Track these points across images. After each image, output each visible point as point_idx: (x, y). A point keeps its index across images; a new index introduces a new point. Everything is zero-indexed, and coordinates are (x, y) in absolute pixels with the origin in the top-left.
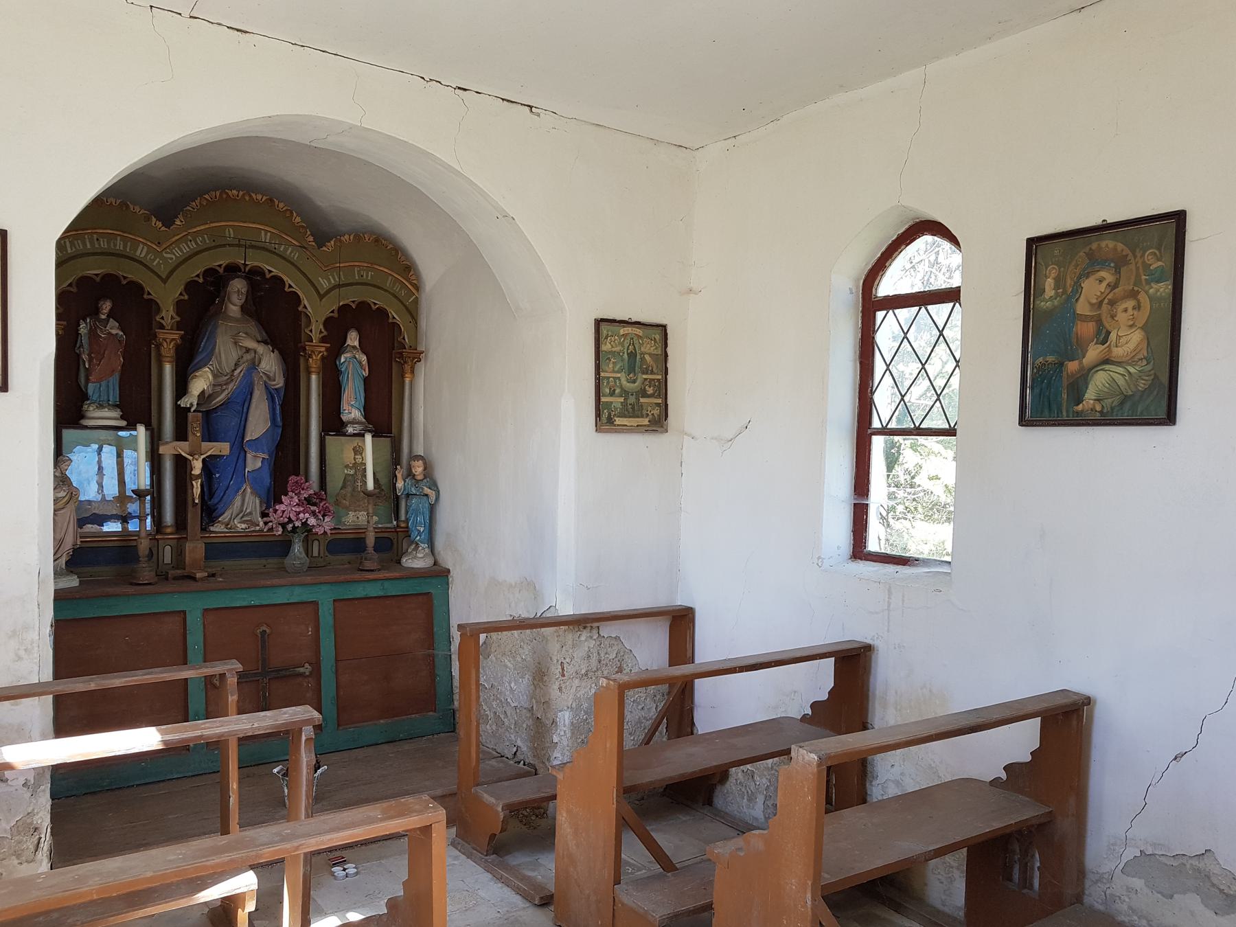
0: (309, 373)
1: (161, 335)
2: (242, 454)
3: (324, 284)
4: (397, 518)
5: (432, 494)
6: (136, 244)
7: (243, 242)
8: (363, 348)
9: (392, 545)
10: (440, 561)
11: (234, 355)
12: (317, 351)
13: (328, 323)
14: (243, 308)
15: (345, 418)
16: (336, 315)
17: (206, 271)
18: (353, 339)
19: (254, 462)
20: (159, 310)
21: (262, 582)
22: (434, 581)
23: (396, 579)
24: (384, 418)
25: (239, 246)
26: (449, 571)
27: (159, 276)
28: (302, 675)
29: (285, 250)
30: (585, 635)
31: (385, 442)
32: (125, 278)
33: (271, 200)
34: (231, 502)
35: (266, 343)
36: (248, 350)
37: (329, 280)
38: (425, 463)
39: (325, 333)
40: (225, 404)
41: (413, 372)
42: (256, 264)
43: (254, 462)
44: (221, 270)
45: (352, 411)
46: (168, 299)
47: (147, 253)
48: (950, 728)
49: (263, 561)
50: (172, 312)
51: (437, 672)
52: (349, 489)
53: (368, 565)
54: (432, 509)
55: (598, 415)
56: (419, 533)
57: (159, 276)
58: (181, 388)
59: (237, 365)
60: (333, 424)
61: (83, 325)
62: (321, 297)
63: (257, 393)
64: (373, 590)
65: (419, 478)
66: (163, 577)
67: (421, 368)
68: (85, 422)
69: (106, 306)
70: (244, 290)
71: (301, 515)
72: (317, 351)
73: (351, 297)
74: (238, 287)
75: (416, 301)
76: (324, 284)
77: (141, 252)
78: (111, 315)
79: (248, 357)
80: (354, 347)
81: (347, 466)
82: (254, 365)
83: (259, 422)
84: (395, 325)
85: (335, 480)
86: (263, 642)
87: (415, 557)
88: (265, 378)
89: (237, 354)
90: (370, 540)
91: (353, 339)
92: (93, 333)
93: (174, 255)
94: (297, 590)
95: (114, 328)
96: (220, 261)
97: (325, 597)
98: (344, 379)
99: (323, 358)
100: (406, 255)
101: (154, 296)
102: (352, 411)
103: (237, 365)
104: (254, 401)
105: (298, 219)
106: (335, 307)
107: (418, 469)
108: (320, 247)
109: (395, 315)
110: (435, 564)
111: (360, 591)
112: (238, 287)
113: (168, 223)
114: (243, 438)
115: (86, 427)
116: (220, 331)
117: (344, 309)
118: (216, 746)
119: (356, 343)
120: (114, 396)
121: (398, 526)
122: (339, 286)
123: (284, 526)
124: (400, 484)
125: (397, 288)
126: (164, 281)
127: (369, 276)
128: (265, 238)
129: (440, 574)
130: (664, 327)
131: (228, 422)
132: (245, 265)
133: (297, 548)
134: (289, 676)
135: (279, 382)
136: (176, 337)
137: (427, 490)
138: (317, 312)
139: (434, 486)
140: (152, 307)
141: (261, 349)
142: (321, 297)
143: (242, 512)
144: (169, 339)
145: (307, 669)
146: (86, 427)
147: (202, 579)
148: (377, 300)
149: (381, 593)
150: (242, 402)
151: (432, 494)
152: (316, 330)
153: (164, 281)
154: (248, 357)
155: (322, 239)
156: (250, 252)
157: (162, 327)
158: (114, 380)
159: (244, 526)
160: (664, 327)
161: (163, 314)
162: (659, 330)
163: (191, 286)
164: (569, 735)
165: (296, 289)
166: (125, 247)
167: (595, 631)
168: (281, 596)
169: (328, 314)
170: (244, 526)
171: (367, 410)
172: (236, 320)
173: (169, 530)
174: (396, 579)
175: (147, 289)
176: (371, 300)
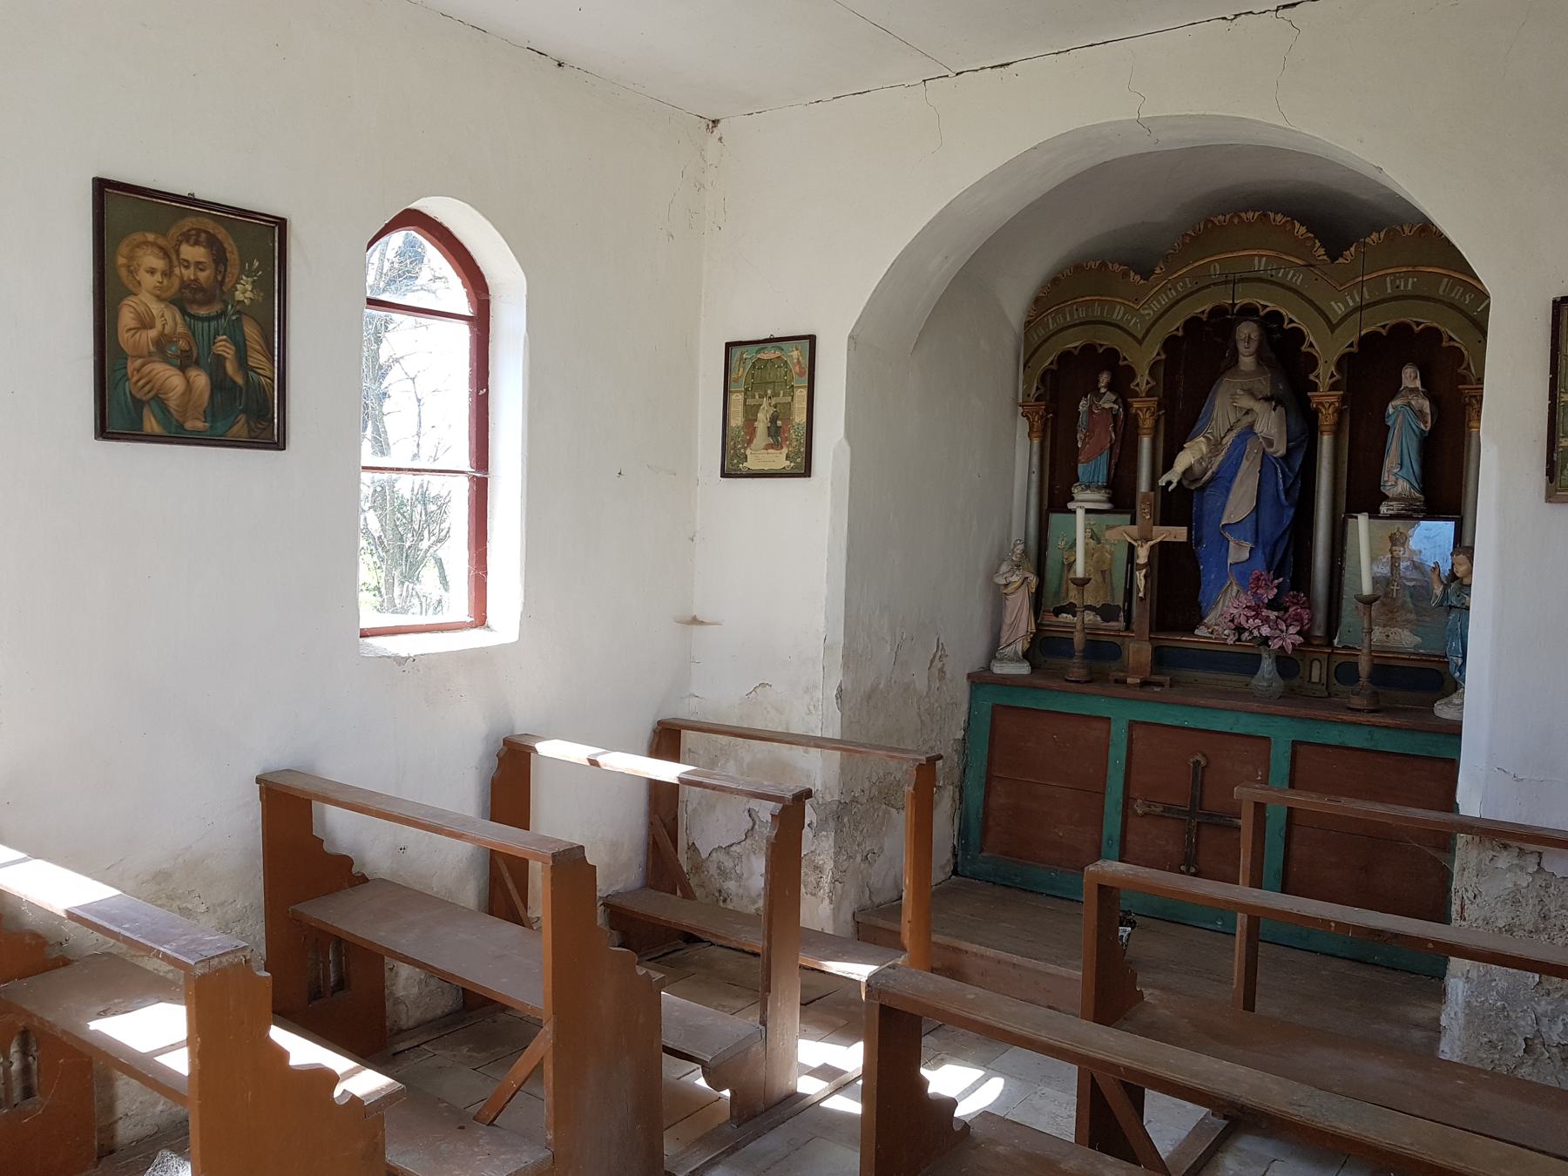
7: (1231, 277)
14: (1259, 355)
16: (1355, 349)
17: (1186, 323)
20: (1134, 376)
25: (1226, 282)
27: (1135, 337)
30: (1504, 860)
37: (1346, 304)
39: (1337, 377)
42: (1246, 301)
43: (1239, 552)
44: (1204, 317)
45: (1398, 480)
46: (1143, 358)
47: (1463, 294)
48: (1194, 1082)
50: (1146, 377)
55: (1551, 473)
57: (1135, 337)
59: (1230, 430)
63: (1245, 464)
64: (1355, 738)
69: (1104, 379)
72: (1326, 400)
73: (1379, 321)
74: (1247, 332)
76: (1339, 309)
77: (1118, 315)
78: (1110, 387)
80: (1413, 390)
83: (1240, 503)
86: (1195, 774)
89: (1242, 417)
90: (1364, 667)
93: (1149, 313)
94: (1244, 718)
95: (1108, 401)
97: (1281, 734)
102: (1398, 480)
103: (1230, 430)
106: (1355, 339)
111: (1333, 735)
112: (1247, 332)
113: (1146, 274)
116: (1221, 390)
118: (1227, 909)
119: (1418, 383)
120: (1102, 478)
125: (1456, 295)
126: (1140, 342)
128: (1259, 265)
130: (729, 346)
132: (1234, 305)
133: (1267, 665)
136: (1333, 399)
138: (1327, 351)
141: (1257, 407)
143: (1227, 611)
144: (1146, 411)
147: (1134, 685)
148: (1422, 318)
150: (1223, 480)
153: (1140, 342)
156: (1239, 287)
157: (1136, 394)
158: (1103, 460)
160: (729, 346)
162: (736, 352)
163: (1170, 344)
164: (1462, 1021)
167: (1534, 859)
169: (1343, 350)
172: (1247, 374)
174: (1398, 728)
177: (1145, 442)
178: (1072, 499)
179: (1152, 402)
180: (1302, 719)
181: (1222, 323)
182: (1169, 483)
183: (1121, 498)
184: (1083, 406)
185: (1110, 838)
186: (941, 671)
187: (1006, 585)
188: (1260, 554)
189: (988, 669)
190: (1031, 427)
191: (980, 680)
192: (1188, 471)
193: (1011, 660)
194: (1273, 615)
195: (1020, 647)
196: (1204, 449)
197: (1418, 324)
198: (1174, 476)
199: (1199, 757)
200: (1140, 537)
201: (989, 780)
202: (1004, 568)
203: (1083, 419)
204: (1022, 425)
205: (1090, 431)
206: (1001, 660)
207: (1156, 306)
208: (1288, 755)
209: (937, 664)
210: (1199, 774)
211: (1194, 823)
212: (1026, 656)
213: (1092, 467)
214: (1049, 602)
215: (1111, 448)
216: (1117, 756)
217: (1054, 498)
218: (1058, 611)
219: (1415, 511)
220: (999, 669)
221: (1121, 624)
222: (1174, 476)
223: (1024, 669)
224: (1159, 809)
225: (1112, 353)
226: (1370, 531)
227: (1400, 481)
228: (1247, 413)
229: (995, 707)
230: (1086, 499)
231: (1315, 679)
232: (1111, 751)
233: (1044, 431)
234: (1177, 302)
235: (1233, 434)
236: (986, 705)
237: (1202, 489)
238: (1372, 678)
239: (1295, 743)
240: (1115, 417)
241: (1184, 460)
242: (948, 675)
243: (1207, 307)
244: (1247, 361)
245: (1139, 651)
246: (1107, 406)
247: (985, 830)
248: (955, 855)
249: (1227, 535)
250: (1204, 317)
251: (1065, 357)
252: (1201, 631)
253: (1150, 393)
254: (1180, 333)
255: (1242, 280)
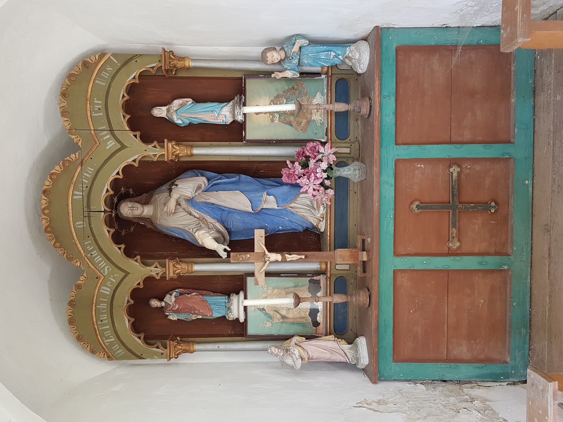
0: (192, 155)
1: (171, 274)
2: (263, 211)
3: (111, 144)
4: (319, 74)
5: (300, 42)
6: (100, 295)
7: (86, 214)
8: (166, 103)
9: (344, 83)
10: (364, 34)
11: (182, 214)
12: (170, 151)
13: (146, 139)
14: (146, 203)
15: (229, 120)
16: (138, 134)
18: (160, 112)
19: (270, 202)
21: (375, 209)
22: (385, 44)
23: (380, 85)
24: (231, 87)
25: (89, 217)
26: (377, 27)
28: (459, 174)
29: (86, 178)
31: (251, 85)
32: (128, 301)
33: (44, 192)
34: (303, 217)
35: (170, 190)
36: (178, 204)
37: (108, 140)
38: (269, 49)
40: (222, 223)
41: (182, 59)
43: (270, 202)
45: (222, 114)
46: (138, 271)
47: (107, 71)
49: (351, 193)
50: (152, 268)
51: (474, 43)
52: (292, 118)
53: (365, 110)
54: (314, 42)
56: (336, 56)
58: (213, 254)
59: (190, 214)
60: (235, 132)
61: (171, 317)
62: (123, 147)
63: (212, 200)
64: (389, 106)
65: (283, 55)
66: (364, 285)
67: (180, 48)
68: (242, 320)
69: (155, 303)
70: (130, 204)
71: (318, 175)
72: (170, 151)
73: (120, 120)
74: (128, 210)
75: (115, 55)
76: (111, 144)
77: (107, 291)
78: (161, 299)
79: (183, 203)
80: (168, 111)
81: (272, 121)
82: (190, 201)
83: (236, 200)
84: (141, 76)
85: (287, 133)
86: (425, 208)
87: (359, 61)
88: (200, 191)
89: (180, 209)
91: (160, 112)
92: (177, 312)
93: (107, 268)
94: (384, 178)
95: (170, 299)
96: (105, 233)
97: (390, 153)
98: (196, 121)
99: (177, 145)
100: (74, 65)
101: (140, 280)
102: (222, 114)
103: (190, 214)
104: (218, 203)
105: (57, 168)
106: (131, 134)
107: (274, 56)
108: (79, 148)
109: (131, 76)
110: (365, 39)
111: (389, 119)
112: (128, 210)
114: (250, 213)
115: (246, 320)
117: (133, 125)
119: (164, 108)
120: (222, 299)
121: (326, 73)
122: (111, 130)
123: (326, 188)
124: (289, 74)
125: (106, 75)
126: (127, 274)
127: (99, 103)
128: (79, 195)
129: (377, 37)
131: (236, 223)
132: (105, 211)
133: (344, 172)
134: (459, 186)
135: (202, 181)
136: (171, 264)
137: (296, 48)
138: (137, 151)
139: (291, 40)
140: (149, 280)
141: (175, 195)
142: (123, 147)
143: (309, 207)
144: (174, 269)
145: (455, 170)
146: (246, 320)
147: (368, 256)
148: (119, 95)
149: (393, 98)
150: (222, 213)
151: (300, 42)
152: (153, 152)
153: (127, 274)
154: (183, 203)
155: (73, 147)
156: (93, 208)
159: (322, 208)
161: (154, 274)
165: (120, 168)
166: (104, 302)
168: (388, 192)
169: (138, 141)
170: (322, 208)
171: (223, 99)
172: (155, 210)
173: (324, 266)
174: (380, 85)
175: (135, 285)
176: (121, 101)
177: (197, 268)
178: (237, 320)
179: (170, 264)
180: (381, 139)
181: (116, 222)
182: (225, 250)
183: (236, 285)
184: (173, 317)
185: (481, 263)
186: (379, 402)
187: (302, 359)
188: (273, 190)
189: (364, 370)
190: (185, 351)
191: (375, 374)
192: (217, 240)
193: (357, 351)
194: (312, 162)
195: (346, 347)
196: (203, 232)
197: (123, 96)
198: (220, 248)
199: (414, 206)
200: (262, 261)
201: (448, 360)
202: (289, 361)
203: (182, 317)
204: (185, 358)
205: (190, 310)
206: (358, 359)
207: (103, 264)
208: (405, 147)
209: (374, 406)
210: (424, 206)
211: (460, 206)
212: (350, 342)
213: (216, 306)
214: (311, 330)
215: (202, 295)
216: (419, 263)
217: (237, 330)
218: (316, 324)
219: (240, 100)
220: (365, 360)
221: (322, 278)
222: (220, 248)
223: (362, 342)
224: (454, 230)
225: (135, 293)
226: (255, 298)
227: (222, 113)
228: (179, 205)
229: (395, 361)
230: (236, 307)
231: (348, 151)
232: (416, 268)
233: (188, 342)
234: (101, 249)
235: (192, 210)
236: (395, 368)
237: (230, 232)
238: (347, 102)
239: (396, 144)
240: (181, 294)
241: (209, 243)
242: (381, 398)
243: (105, 229)
244: (147, 211)
245: (342, 260)
246: (173, 299)
247: (488, 361)
248: (514, 384)
249: (259, 209)
250: (112, 231)
251: (136, 328)
252: (322, 227)
253: (163, 266)
254: (123, 246)
255: (88, 206)
